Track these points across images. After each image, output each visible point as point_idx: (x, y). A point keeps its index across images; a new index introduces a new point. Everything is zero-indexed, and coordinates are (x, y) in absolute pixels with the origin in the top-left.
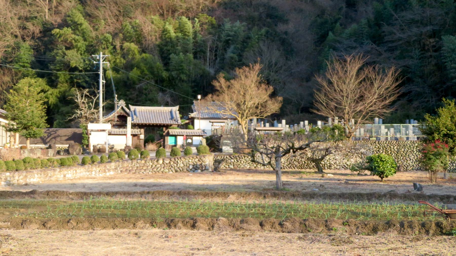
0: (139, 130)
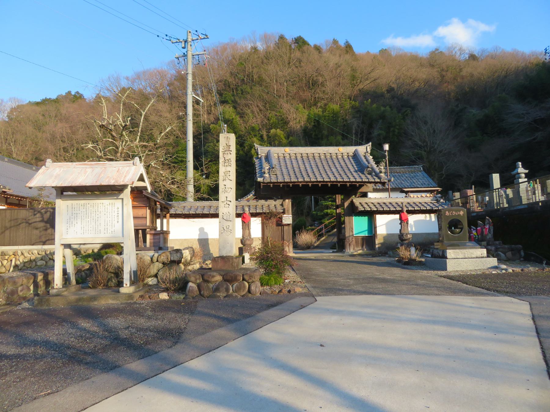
0: (279, 202)
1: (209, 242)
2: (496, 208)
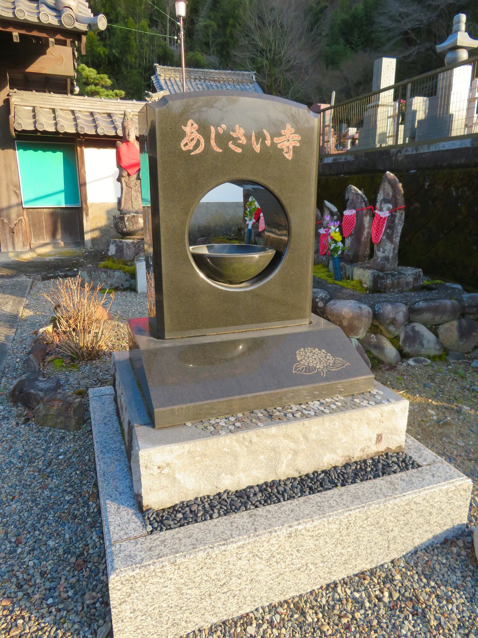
1: (11, 151)
2: (378, 146)
